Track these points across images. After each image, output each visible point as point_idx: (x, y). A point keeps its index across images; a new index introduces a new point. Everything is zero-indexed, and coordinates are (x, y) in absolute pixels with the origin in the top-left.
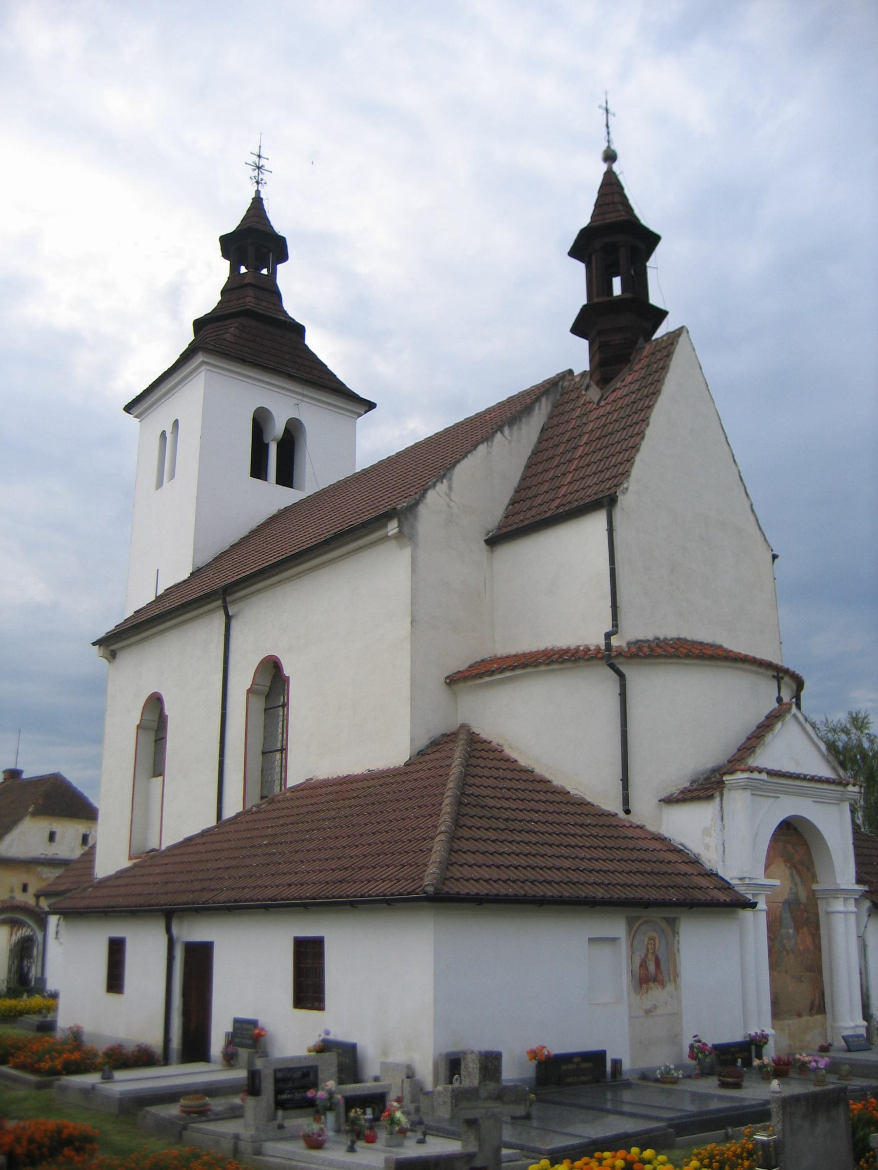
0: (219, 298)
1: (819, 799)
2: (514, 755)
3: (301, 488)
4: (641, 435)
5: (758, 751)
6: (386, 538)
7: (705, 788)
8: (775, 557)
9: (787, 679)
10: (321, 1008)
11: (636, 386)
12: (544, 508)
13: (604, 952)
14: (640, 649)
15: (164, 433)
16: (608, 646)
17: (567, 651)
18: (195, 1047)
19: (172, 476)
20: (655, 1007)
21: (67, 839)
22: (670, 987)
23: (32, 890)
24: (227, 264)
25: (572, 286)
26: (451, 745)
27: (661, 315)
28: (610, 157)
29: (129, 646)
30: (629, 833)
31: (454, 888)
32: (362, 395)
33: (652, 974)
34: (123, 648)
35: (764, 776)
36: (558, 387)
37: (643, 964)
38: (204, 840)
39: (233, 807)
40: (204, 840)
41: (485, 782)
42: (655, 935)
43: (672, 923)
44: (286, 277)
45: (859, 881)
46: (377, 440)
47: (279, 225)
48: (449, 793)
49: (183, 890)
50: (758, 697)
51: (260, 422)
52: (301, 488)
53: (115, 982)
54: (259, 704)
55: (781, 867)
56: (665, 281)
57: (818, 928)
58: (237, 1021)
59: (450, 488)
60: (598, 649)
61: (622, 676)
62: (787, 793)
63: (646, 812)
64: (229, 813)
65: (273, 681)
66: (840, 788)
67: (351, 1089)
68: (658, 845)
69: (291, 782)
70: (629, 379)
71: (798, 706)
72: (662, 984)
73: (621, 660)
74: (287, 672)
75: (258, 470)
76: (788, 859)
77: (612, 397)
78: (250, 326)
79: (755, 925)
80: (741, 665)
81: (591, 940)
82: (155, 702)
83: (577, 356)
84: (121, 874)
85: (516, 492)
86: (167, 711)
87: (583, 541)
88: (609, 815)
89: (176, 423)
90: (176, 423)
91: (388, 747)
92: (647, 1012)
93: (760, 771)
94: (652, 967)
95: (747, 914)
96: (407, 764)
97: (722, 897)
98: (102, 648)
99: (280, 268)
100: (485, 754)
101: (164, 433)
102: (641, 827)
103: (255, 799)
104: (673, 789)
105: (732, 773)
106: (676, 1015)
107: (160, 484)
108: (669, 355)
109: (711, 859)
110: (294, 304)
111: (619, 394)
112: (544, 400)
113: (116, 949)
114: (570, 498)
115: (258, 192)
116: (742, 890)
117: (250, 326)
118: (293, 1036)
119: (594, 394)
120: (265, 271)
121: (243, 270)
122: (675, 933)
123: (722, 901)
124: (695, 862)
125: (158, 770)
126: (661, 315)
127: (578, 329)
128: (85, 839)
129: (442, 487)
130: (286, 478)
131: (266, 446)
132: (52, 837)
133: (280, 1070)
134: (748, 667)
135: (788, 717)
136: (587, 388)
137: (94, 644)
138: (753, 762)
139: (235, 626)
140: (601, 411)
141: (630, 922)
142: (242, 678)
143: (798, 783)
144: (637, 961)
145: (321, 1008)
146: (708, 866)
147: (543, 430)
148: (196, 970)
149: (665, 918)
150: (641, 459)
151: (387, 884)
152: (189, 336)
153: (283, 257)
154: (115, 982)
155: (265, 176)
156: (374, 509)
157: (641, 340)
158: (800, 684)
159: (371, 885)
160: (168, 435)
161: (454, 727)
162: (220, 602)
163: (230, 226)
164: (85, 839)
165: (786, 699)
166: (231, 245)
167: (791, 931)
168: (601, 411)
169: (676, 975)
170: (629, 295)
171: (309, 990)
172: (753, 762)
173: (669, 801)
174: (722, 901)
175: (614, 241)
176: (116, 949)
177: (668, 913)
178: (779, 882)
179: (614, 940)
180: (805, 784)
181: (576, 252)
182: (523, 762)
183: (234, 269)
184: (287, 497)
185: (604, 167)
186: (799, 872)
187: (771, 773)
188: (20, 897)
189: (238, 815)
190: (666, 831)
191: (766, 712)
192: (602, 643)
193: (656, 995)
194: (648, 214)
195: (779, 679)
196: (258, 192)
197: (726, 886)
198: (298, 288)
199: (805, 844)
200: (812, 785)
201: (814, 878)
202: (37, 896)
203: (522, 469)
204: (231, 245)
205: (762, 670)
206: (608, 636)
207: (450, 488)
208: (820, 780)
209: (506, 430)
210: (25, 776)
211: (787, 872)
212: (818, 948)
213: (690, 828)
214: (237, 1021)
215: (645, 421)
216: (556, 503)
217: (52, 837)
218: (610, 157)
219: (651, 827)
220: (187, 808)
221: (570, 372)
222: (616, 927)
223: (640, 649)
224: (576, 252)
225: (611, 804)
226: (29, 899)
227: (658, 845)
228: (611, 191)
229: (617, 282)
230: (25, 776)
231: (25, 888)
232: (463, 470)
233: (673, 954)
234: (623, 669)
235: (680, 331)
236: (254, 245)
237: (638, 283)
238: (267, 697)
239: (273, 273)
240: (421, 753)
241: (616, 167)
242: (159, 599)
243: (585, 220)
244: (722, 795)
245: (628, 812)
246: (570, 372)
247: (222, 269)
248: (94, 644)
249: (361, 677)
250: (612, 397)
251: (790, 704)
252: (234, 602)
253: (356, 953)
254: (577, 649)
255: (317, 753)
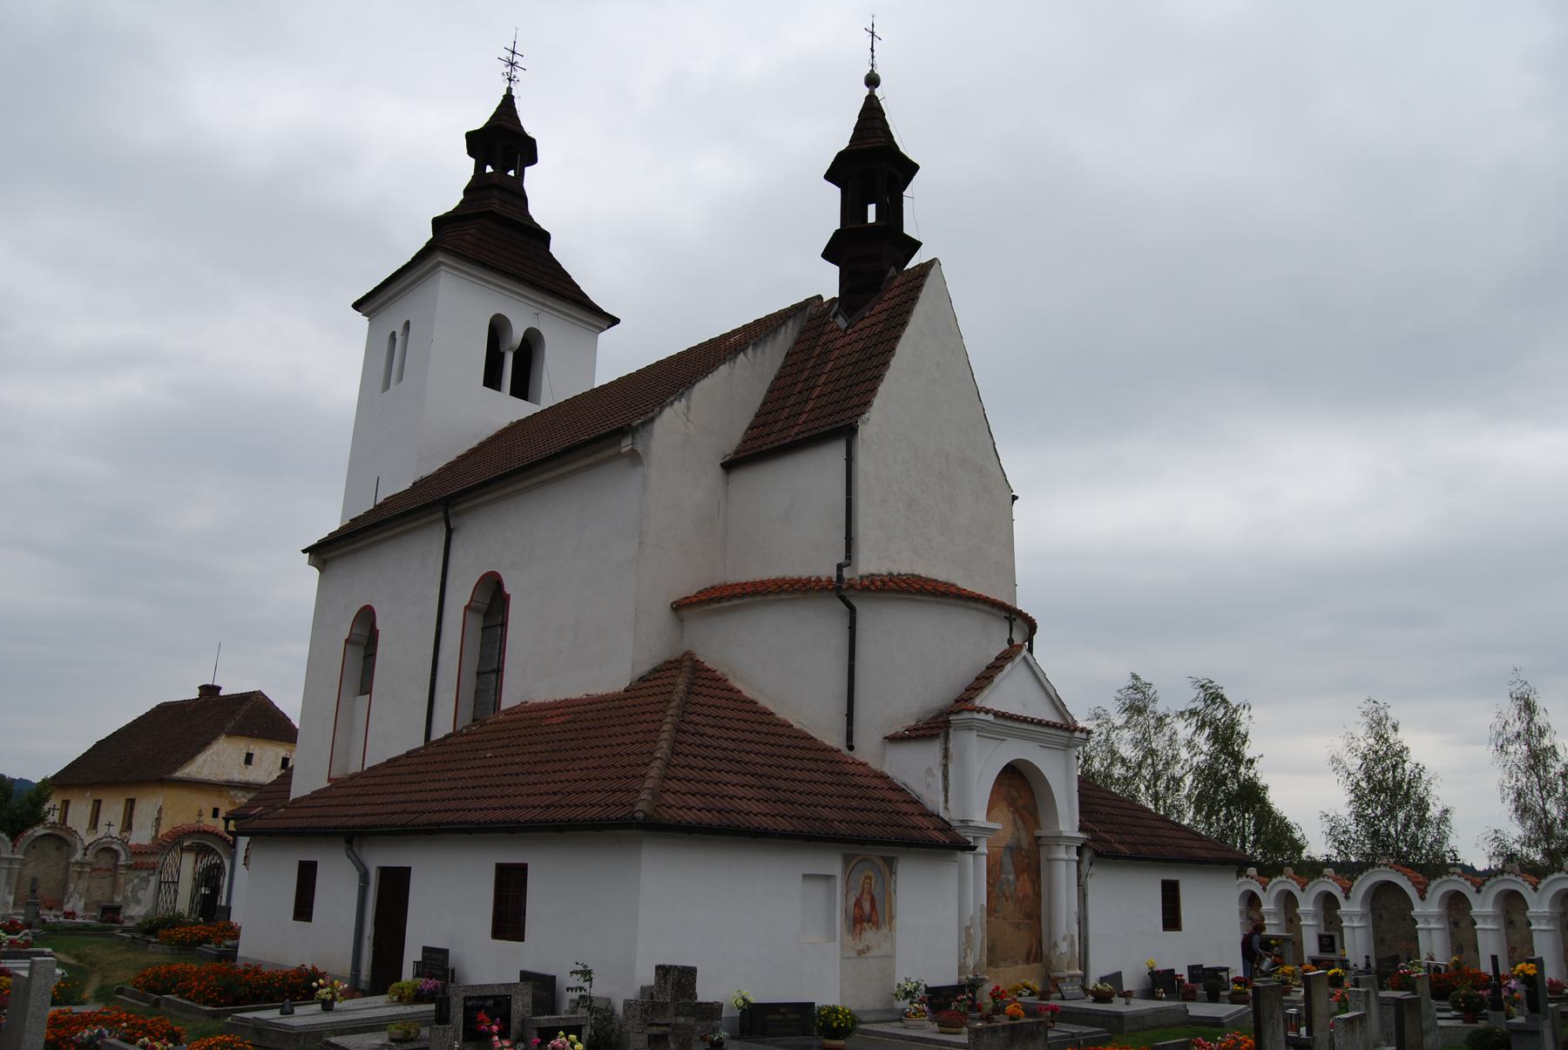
0: (462, 197)
1: (1045, 744)
2: (738, 685)
3: (537, 402)
4: (886, 364)
5: (986, 692)
6: (619, 456)
7: (933, 728)
8: (1015, 498)
9: (1019, 621)
10: (522, 940)
11: (883, 316)
12: (784, 434)
13: (819, 889)
14: (873, 582)
15: (393, 334)
16: (840, 577)
17: (799, 581)
18: (384, 973)
19: (400, 379)
20: (869, 948)
21: (266, 763)
22: (885, 930)
23: (222, 814)
24: (471, 163)
25: (824, 210)
26: (674, 672)
27: (916, 245)
28: (872, 81)
29: (342, 555)
30: (852, 769)
31: (667, 815)
32: (595, 298)
33: (867, 915)
34: (333, 559)
35: (990, 717)
36: (808, 313)
37: (858, 904)
38: (409, 761)
39: (443, 726)
40: (409, 761)
41: (705, 710)
42: (871, 873)
43: (890, 862)
44: (534, 180)
45: (1081, 829)
46: (616, 357)
47: (530, 127)
48: (669, 719)
49: (380, 815)
50: (996, 639)
51: (497, 329)
52: (537, 402)
53: (303, 909)
54: (476, 622)
55: (1004, 811)
56: (921, 212)
57: (1039, 876)
58: (426, 949)
59: (688, 408)
60: (830, 580)
61: (852, 610)
62: (1013, 736)
63: (868, 749)
64: (437, 735)
65: (492, 601)
66: (1066, 734)
67: (545, 1019)
68: (875, 782)
69: (506, 704)
70: (878, 308)
71: (1030, 650)
72: (877, 925)
73: (852, 592)
74: (508, 589)
75: (492, 379)
76: (1012, 804)
77: (860, 325)
78: (492, 226)
79: (975, 868)
80: (972, 604)
81: (805, 876)
82: (366, 617)
83: (826, 282)
84: (316, 795)
85: (757, 416)
86: (378, 626)
87: (819, 470)
88: (832, 750)
89: (407, 324)
90: (407, 324)
91: (611, 675)
92: (861, 953)
93: (987, 712)
94: (867, 906)
95: (969, 857)
96: (626, 690)
97: (941, 837)
98: (738, 1013)
99: (528, 170)
100: (708, 683)
101: (393, 334)
102: (865, 765)
103: (466, 719)
104: (898, 728)
105: (958, 712)
106: (890, 957)
107: (386, 387)
108: (919, 287)
109: (933, 798)
110: (541, 209)
111: (866, 323)
112: (790, 323)
113: (307, 874)
114: (810, 425)
115: (509, 89)
116: (962, 832)
117: (492, 226)
118: (488, 964)
119: (841, 322)
120: (511, 173)
121: (489, 169)
122: (892, 872)
123: (946, 842)
124: (916, 802)
125: (366, 687)
126: (916, 245)
127: (829, 254)
128: (285, 761)
129: (679, 406)
130: (521, 389)
131: (502, 356)
132: (249, 759)
133: (471, 998)
134: (980, 606)
135: (1019, 658)
136: (835, 316)
137: (304, 551)
138: (978, 702)
139: (454, 536)
140: (847, 339)
141: (847, 859)
142: (461, 594)
143: (1024, 726)
144: (852, 901)
145: (522, 940)
146: (930, 806)
147: (788, 355)
148: (392, 895)
149: (883, 858)
150: (882, 389)
151: (596, 810)
152: (428, 234)
153: (532, 159)
154: (303, 909)
155: (518, 73)
156: (610, 424)
157: (893, 271)
158: (1031, 626)
159: (580, 810)
160: (398, 336)
161: (678, 654)
162: (441, 515)
163: (479, 121)
164: (285, 761)
165: (1017, 641)
166: (476, 142)
167: (1011, 877)
168: (847, 339)
169: (892, 918)
170: (883, 223)
171: (509, 920)
172: (978, 702)
173: (894, 739)
174: (946, 842)
175: (872, 167)
176: (307, 874)
177: (888, 852)
178: (1001, 825)
179: (828, 878)
180: (1032, 727)
181: (830, 176)
182: (748, 693)
183: (479, 168)
184: (522, 409)
185: (866, 91)
186: (1022, 817)
187: (997, 714)
188: (208, 822)
189: (447, 737)
190: (887, 771)
191: (996, 654)
192: (833, 574)
193: (870, 936)
194: (907, 142)
195: (1011, 621)
196: (509, 89)
197: (946, 827)
198: (546, 194)
199: (1030, 789)
200: (1039, 729)
201: (1037, 824)
202: (227, 820)
203: (752, 417)
204: (476, 142)
205: (995, 611)
206: (840, 567)
207: (688, 408)
208: (1047, 725)
209: (750, 350)
210: (222, 693)
211: (1010, 816)
212: (1038, 895)
213: (913, 769)
214: (426, 949)
215: (891, 351)
216: (796, 429)
217: (249, 759)
218: (872, 81)
219: (874, 765)
220: (395, 727)
221: (820, 297)
222: (832, 865)
223: (873, 582)
224: (830, 176)
225: (833, 738)
226: (219, 825)
227: (875, 782)
228: (872, 115)
229: (872, 210)
230: (222, 693)
231: (215, 813)
232: (705, 388)
233: (889, 894)
234: (854, 602)
235: (932, 262)
236: (502, 145)
237: (893, 212)
238: (486, 615)
239: (520, 176)
240: (642, 679)
241: (878, 92)
242: (378, 508)
243: (843, 143)
244: (947, 738)
245: (851, 748)
246: (820, 297)
247: (464, 168)
248: (304, 551)
249: (587, 605)
250: (860, 325)
251: (1021, 647)
252: (457, 514)
253: (561, 887)
254: (809, 580)
255: (538, 674)
